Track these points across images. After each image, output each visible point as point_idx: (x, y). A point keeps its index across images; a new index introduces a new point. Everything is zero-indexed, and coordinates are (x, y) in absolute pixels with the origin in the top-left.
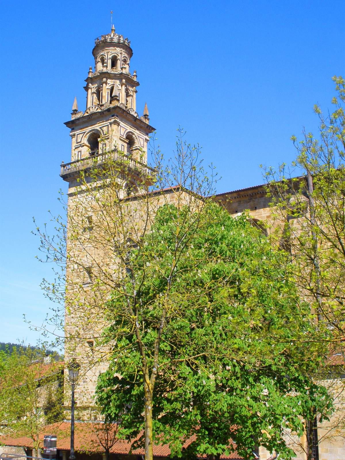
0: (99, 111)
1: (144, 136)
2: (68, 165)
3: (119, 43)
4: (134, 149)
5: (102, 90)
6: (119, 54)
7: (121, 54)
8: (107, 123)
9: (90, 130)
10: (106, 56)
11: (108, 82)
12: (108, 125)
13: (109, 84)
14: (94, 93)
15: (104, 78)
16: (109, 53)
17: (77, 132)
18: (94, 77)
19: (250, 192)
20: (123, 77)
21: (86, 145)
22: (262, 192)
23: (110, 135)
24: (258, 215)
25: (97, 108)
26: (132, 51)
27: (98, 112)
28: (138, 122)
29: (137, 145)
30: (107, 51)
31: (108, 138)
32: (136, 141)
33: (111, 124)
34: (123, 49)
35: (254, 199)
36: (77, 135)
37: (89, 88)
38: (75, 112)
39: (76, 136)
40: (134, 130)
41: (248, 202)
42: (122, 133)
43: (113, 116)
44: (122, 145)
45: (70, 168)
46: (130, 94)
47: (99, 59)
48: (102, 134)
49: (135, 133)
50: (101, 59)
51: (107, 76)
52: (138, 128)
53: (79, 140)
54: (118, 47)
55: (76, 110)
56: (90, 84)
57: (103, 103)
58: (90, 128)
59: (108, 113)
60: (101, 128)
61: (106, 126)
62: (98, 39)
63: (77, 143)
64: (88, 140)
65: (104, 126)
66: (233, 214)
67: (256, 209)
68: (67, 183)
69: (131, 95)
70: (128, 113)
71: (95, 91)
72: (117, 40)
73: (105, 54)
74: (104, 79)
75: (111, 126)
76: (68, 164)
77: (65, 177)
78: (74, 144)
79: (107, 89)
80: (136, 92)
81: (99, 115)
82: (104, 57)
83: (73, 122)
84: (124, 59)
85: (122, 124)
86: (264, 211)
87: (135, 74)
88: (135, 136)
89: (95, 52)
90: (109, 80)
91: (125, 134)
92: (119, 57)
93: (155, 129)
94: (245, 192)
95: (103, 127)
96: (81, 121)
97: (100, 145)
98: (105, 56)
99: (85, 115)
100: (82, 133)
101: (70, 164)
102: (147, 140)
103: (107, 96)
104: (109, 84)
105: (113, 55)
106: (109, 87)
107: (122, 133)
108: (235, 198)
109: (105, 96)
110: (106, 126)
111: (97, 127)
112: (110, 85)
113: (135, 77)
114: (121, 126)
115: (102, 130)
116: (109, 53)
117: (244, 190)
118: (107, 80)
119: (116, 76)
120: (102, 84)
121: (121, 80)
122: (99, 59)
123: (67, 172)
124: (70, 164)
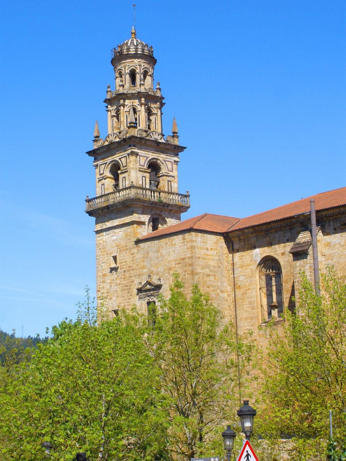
1: (172, 158)
4: (160, 175)
9: (111, 160)
10: (124, 70)
12: (126, 156)
13: (127, 105)
14: (113, 116)
16: (127, 67)
17: (100, 162)
19: (264, 227)
20: (141, 96)
21: (108, 178)
24: (274, 252)
28: (161, 145)
30: (124, 65)
31: (127, 171)
32: (162, 166)
34: (142, 59)
35: (270, 234)
36: (100, 165)
40: (158, 155)
41: (265, 237)
42: (142, 163)
43: (130, 146)
48: (122, 166)
49: (159, 158)
51: (123, 97)
53: (102, 172)
54: (135, 58)
58: (109, 159)
59: (125, 143)
60: (120, 159)
63: (100, 175)
65: (123, 157)
66: (252, 249)
68: (93, 219)
69: (154, 114)
72: (134, 50)
74: (122, 101)
75: (129, 157)
79: (125, 112)
81: (117, 145)
85: (141, 152)
86: (279, 248)
87: (158, 87)
88: (161, 161)
90: (127, 101)
91: (146, 162)
92: (138, 71)
93: (185, 148)
98: (122, 70)
99: (105, 145)
101: (96, 198)
105: (131, 68)
107: (142, 162)
108: (252, 233)
109: (124, 120)
111: (116, 157)
112: (128, 106)
113: (158, 91)
114: (140, 156)
116: (127, 66)
117: (258, 226)
118: (124, 101)
119: (134, 96)
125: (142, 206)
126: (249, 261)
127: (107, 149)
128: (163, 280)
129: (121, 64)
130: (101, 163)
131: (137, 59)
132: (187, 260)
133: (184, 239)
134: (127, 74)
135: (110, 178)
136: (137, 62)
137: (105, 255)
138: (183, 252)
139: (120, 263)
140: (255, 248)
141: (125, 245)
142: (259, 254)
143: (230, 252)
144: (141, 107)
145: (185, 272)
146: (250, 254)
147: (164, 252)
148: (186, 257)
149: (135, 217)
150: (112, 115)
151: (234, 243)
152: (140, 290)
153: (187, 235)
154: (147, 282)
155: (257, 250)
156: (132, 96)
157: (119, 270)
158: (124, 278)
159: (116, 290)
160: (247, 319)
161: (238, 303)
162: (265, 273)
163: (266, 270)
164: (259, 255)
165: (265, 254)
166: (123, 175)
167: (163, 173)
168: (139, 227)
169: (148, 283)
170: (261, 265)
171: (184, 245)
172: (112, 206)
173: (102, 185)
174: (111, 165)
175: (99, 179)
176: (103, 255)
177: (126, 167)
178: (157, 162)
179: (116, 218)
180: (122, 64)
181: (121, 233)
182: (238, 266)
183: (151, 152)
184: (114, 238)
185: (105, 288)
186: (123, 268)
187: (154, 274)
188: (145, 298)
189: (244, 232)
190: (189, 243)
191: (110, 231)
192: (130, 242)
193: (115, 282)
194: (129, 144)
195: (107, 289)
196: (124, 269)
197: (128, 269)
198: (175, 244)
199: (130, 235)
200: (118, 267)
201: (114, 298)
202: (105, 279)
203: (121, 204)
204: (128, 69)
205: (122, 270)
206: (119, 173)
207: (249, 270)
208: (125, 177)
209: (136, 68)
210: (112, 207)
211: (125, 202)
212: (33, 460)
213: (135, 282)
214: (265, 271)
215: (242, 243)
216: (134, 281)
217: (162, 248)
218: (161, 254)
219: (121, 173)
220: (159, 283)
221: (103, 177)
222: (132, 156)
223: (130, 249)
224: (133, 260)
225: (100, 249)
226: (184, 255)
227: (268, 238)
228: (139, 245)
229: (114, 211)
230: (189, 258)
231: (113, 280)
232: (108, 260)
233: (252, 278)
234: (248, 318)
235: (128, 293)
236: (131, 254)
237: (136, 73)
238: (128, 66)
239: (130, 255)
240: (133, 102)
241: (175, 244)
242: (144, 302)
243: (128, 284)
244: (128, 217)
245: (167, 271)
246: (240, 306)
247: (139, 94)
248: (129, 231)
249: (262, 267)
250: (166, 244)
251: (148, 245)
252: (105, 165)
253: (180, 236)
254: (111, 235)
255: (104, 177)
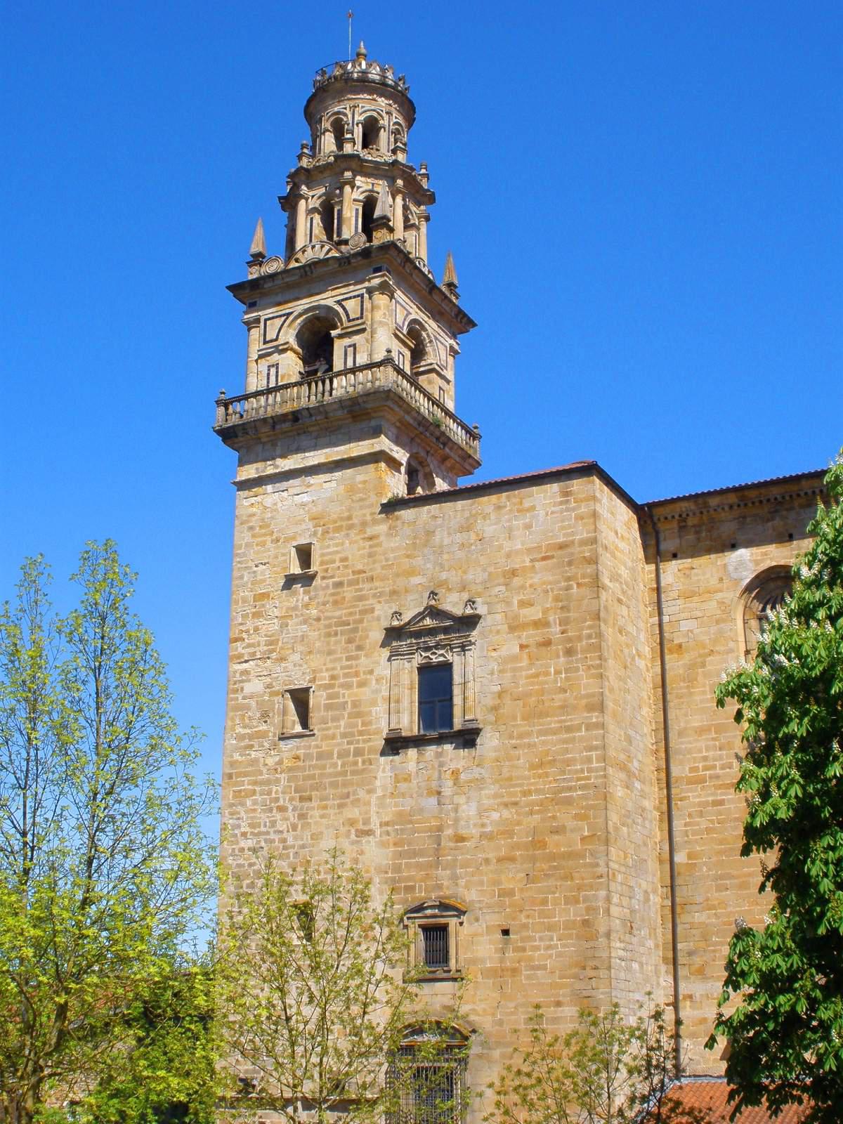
0: (334, 254)
1: (448, 339)
2: (239, 401)
3: (385, 84)
4: (422, 369)
5: (341, 202)
6: (384, 114)
7: (389, 113)
8: (361, 288)
9: (302, 308)
10: (350, 116)
11: (358, 183)
12: (362, 296)
13: (358, 187)
15: (347, 170)
17: (265, 314)
18: (316, 168)
19: (776, 491)
21: (292, 349)
22: (810, 492)
23: (369, 323)
25: (327, 248)
26: (415, 112)
27: (333, 258)
28: (436, 297)
29: (431, 359)
30: (352, 103)
31: (364, 330)
32: (429, 349)
33: (370, 291)
34: (395, 103)
35: (784, 513)
36: (266, 320)
37: (302, 197)
38: (258, 259)
39: (262, 324)
41: (768, 520)
42: (400, 321)
43: (377, 270)
44: (400, 353)
45: (246, 408)
46: (412, 222)
47: (326, 124)
48: (344, 318)
49: (426, 325)
50: (332, 125)
51: (354, 165)
52: (437, 315)
53: (271, 335)
55: (260, 255)
56: (304, 187)
57: (345, 235)
60: (339, 302)
61: (355, 297)
62: (324, 73)
63: (265, 342)
64: (297, 336)
65: (350, 298)
66: (723, 551)
67: (791, 538)
70: (417, 268)
71: (317, 205)
73: (347, 111)
75: (370, 298)
76: (240, 399)
77: (228, 435)
78: (255, 348)
79: (355, 200)
80: (427, 219)
81: (336, 266)
82: (342, 120)
83: (255, 284)
84: (396, 129)
85: (399, 294)
87: (423, 171)
89: (311, 114)
90: (358, 178)
91: (406, 323)
93: (474, 325)
94: (763, 491)
95: (346, 299)
96: (278, 282)
97: (339, 347)
98: (345, 115)
100: (281, 316)
101: (246, 397)
102: (453, 352)
103: (354, 219)
104: (358, 187)
105: (369, 114)
106: (358, 195)
108: (731, 507)
109: (350, 219)
110: (355, 297)
111: (328, 299)
112: (360, 190)
114: (397, 302)
115: (344, 309)
118: (354, 176)
119: (379, 169)
120: (341, 189)
121: (393, 182)
122: (326, 124)
123: (234, 420)
124: (246, 397)
125: (400, 421)
126: (714, 582)
127: (301, 276)
128: (484, 603)
129: (343, 101)
130: (271, 316)
131: (383, 99)
132: (576, 549)
133: (566, 494)
134: (357, 124)
135: (295, 352)
136: (383, 105)
137: (269, 544)
138: (563, 528)
139: (322, 563)
140: (734, 547)
141: (346, 514)
142: (748, 563)
143: (648, 560)
144: (394, 199)
145: (569, 579)
146: (719, 563)
147: (489, 529)
148: (573, 542)
149: (384, 443)
150: (310, 207)
151: (662, 536)
152: (394, 634)
153: (577, 485)
154: (426, 609)
155: (743, 553)
156: (375, 170)
157: (317, 582)
158: (336, 603)
159: (303, 636)
160: (701, 731)
161: (672, 689)
162: (758, 613)
163: (761, 606)
164: (751, 566)
165: (769, 561)
166: (347, 341)
167: (431, 364)
168: (389, 472)
169: (434, 612)
170: (751, 592)
171: (567, 510)
172: (312, 412)
173: (269, 366)
174: (304, 320)
175: (260, 353)
176: (263, 544)
177: (360, 321)
178: (421, 335)
179: (315, 447)
180: (346, 102)
181: (334, 484)
182: (674, 594)
183: (415, 304)
184: (305, 498)
185: (262, 632)
186: (332, 577)
187: (449, 590)
188: (414, 654)
189: (706, 505)
190: (583, 504)
191: (291, 481)
192: (361, 508)
193: (302, 615)
194: (375, 267)
195: (270, 633)
196: (336, 579)
197: (351, 577)
198: (533, 508)
199: (364, 488)
200: (317, 572)
201: (296, 657)
202: (263, 606)
203: (342, 407)
204: (361, 114)
205: (331, 581)
206: (332, 335)
207: (715, 603)
208: (354, 346)
209: (381, 116)
210: (311, 415)
211: (360, 400)
212: (220, 1119)
213: (376, 613)
214: (760, 608)
215: (691, 537)
216: (374, 608)
217: (484, 518)
218: (478, 535)
219: (340, 336)
220: (469, 611)
221: (277, 347)
222: (383, 294)
223: (364, 524)
224: (370, 555)
225: (251, 528)
226: (565, 535)
227: (777, 522)
228: (397, 513)
229: (311, 429)
230: (583, 543)
231: (295, 608)
232: (276, 557)
233: (722, 625)
234: (710, 730)
235: (350, 641)
236: (364, 539)
237: (381, 128)
238: (363, 107)
239: (361, 542)
240: (373, 184)
241: (533, 508)
242: (407, 665)
243: (351, 618)
244: (360, 443)
245: (502, 580)
246: (679, 697)
247: (393, 166)
248: (360, 478)
249: (754, 598)
250: (499, 508)
251: (429, 512)
252: (283, 319)
253: (554, 488)
254: (292, 491)
255: (281, 348)
